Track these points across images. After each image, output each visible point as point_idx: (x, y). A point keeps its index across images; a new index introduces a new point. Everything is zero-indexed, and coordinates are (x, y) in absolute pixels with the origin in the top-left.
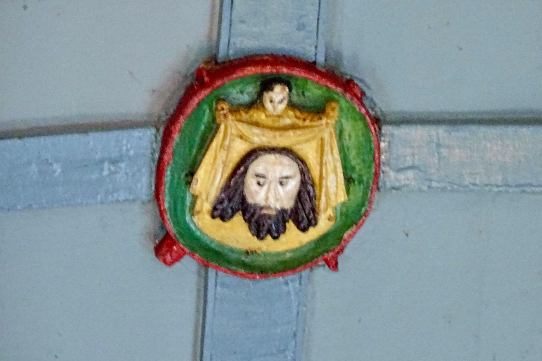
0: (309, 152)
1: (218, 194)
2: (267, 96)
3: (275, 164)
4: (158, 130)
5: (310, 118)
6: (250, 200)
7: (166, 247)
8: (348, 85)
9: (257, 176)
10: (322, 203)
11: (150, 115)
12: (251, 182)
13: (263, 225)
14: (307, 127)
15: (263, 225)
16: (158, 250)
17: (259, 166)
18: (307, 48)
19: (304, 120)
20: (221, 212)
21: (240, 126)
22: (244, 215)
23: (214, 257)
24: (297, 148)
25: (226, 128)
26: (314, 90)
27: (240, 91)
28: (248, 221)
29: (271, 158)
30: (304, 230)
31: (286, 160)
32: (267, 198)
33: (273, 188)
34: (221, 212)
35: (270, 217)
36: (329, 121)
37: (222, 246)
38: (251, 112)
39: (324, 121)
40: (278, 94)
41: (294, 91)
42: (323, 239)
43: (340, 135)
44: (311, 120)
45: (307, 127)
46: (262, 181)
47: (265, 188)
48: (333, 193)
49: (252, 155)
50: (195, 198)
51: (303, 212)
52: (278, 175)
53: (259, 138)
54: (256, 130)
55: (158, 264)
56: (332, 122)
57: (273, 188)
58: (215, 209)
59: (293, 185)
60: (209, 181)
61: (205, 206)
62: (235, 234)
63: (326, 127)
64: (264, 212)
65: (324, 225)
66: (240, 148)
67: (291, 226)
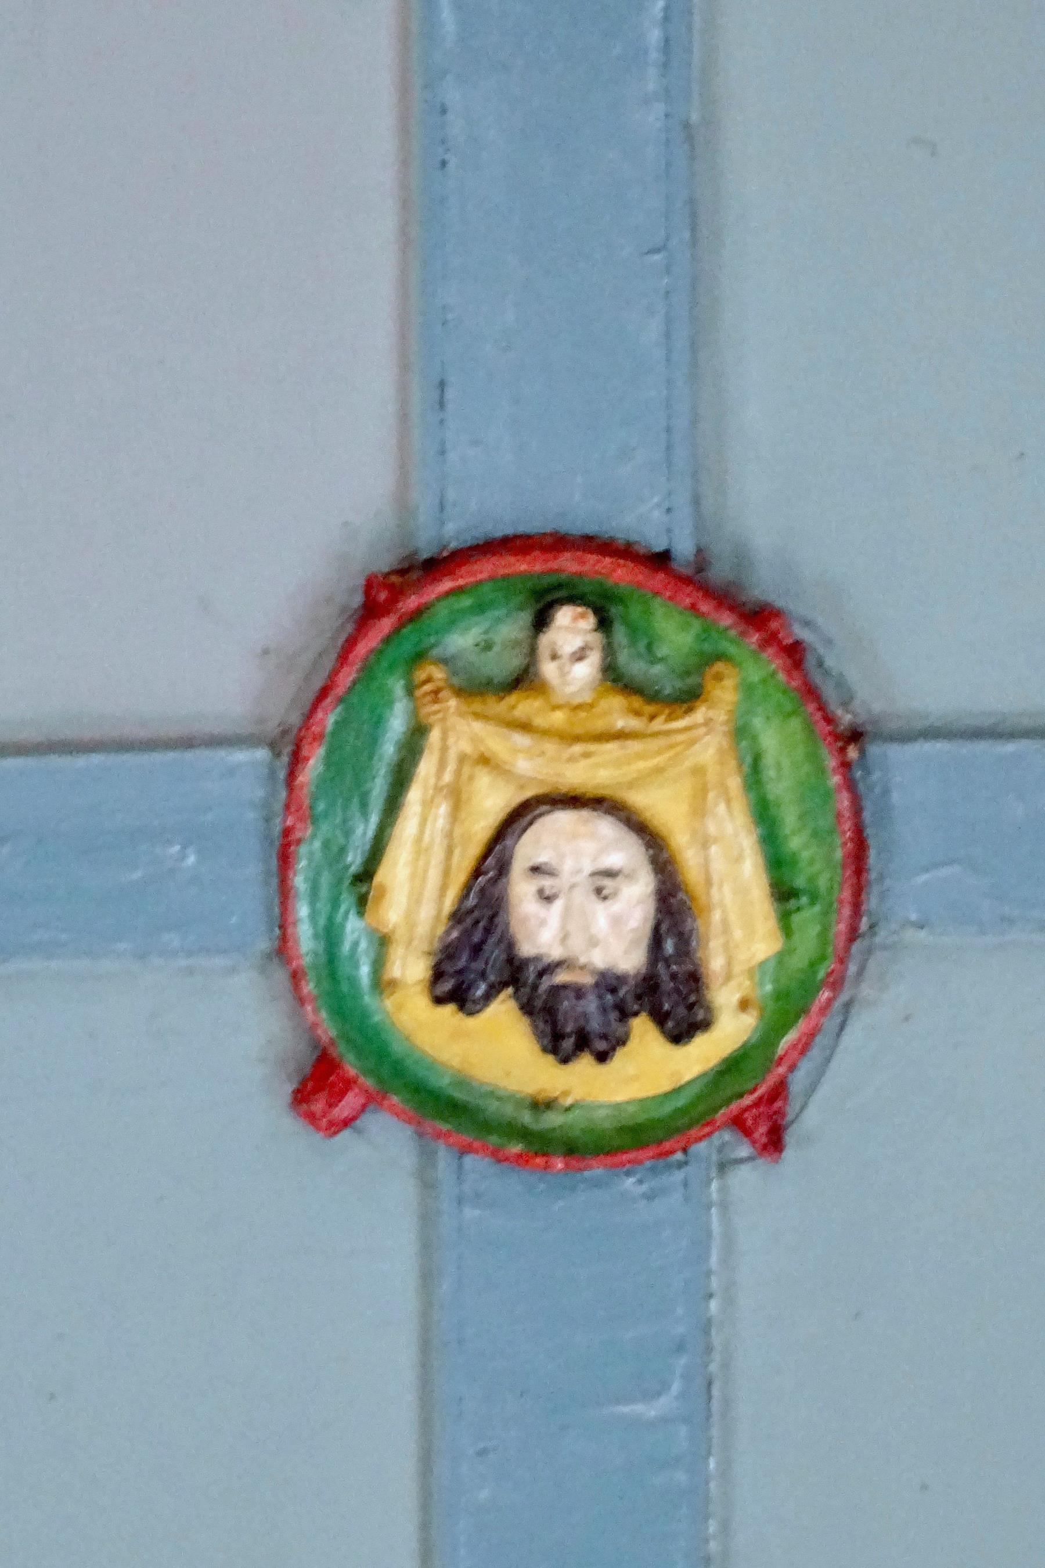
0: (664, 805)
1: (441, 930)
2: (546, 639)
3: (574, 836)
4: (277, 755)
5: (667, 711)
6: (526, 949)
7: (324, 1085)
8: (760, 619)
9: (536, 870)
10: (715, 962)
11: (261, 721)
12: (521, 890)
13: (571, 1022)
14: (656, 734)
15: (571, 1022)
16: (301, 1097)
17: (536, 844)
18: (647, 518)
19: (652, 718)
20: (457, 983)
21: (478, 726)
22: (516, 995)
23: (449, 1113)
24: (639, 799)
25: (444, 738)
26: (675, 631)
27: (473, 633)
28: (527, 1008)
29: (563, 819)
30: (679, 1036)
31: (606, 827)
32: (564, 938)
33: (584, 915)
34: (457, 983)
35: (579, 992)
36: (711, 714)
37: (462, 1081)
38: (512, 699)
39: (699, 715)
40: (571, 628)
41: (620, 633)
42: (732, 1066)
43: (754, 776)
44: (670, 718)
45: (656, 734)
46: (546, 882)
47: (558, 905)
48: (742, 941)
49: (518, 818)
50: (383, 942)
51: (669, 992)
52: (588, 867)
53: (534, 765)
54: (521, 740)
55: (291, 1124)
56: (720, 715)
57: (584, 915)
58: (438, 974)
59: (636, 899)
60: (415, 895)
61: (411, 968)
62: (495, 1049)
63: (703, 739)
64: (561, 977)
65: (730, 1030)
66: (492, 802)
67: (642, 1026)
